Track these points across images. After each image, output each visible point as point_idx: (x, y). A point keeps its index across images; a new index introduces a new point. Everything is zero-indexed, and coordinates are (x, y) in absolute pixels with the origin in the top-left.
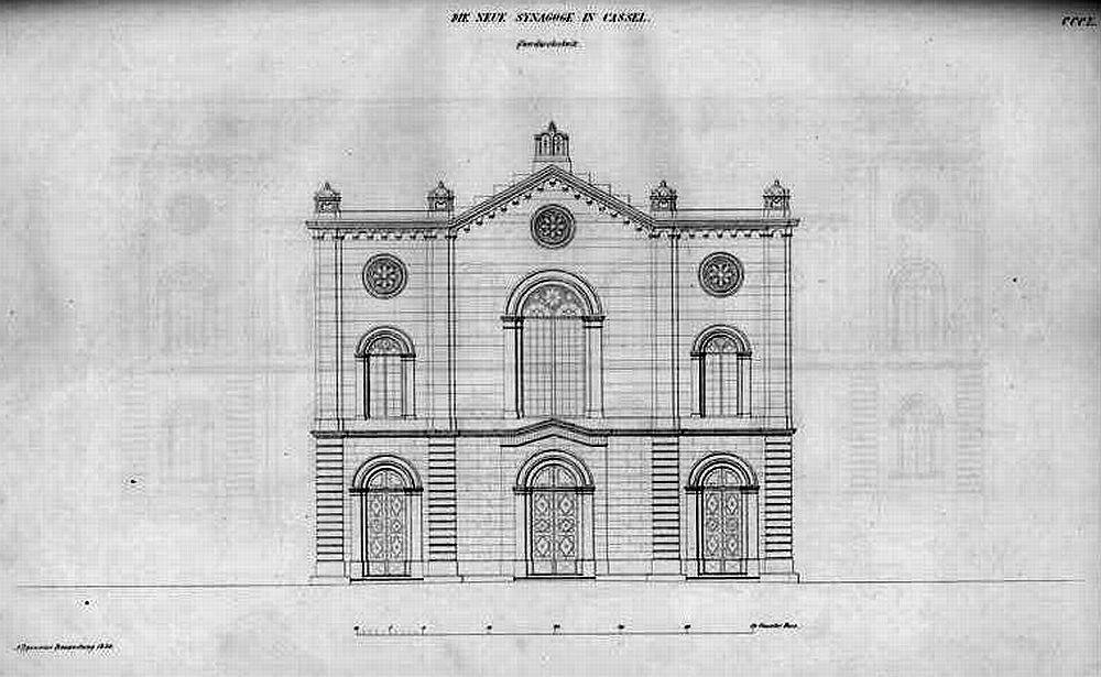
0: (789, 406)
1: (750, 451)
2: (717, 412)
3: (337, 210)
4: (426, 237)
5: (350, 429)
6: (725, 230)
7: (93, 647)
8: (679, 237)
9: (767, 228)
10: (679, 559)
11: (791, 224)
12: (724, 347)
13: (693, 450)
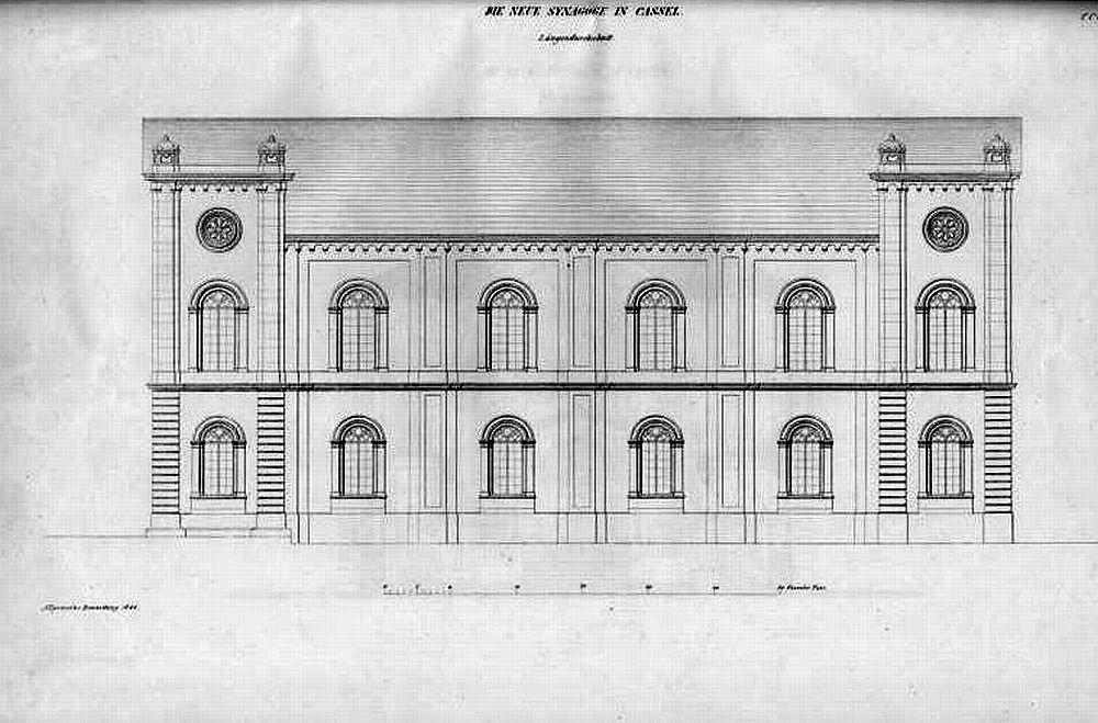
0: (1008, 361)
1: (970, 409)
2: (801, 367)
3: (175, 163)
4: (984, 189)
5: (761, 381)
6: (250, 184)
7: (117, 608)
8: (180, 190)
9: (262, 182)
10: (906, 513)
11: (1012, 177)
12: (948, 301)
13: (922, 409)
